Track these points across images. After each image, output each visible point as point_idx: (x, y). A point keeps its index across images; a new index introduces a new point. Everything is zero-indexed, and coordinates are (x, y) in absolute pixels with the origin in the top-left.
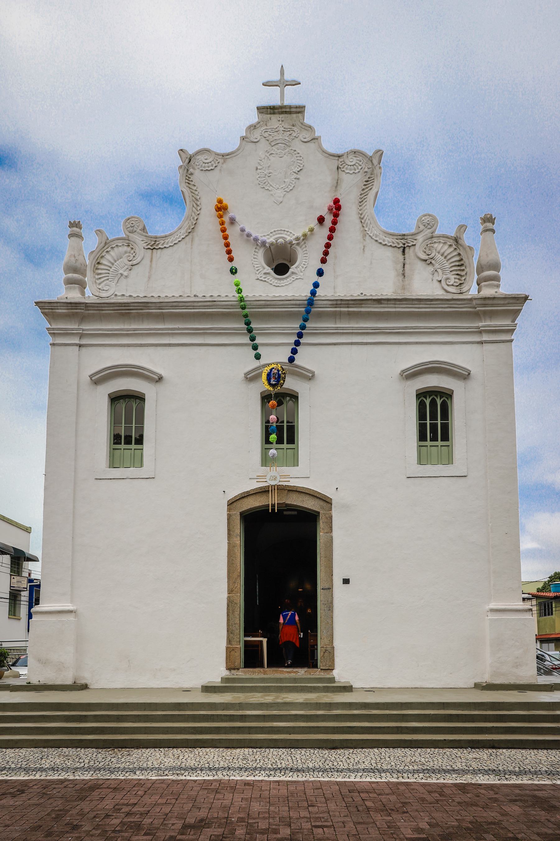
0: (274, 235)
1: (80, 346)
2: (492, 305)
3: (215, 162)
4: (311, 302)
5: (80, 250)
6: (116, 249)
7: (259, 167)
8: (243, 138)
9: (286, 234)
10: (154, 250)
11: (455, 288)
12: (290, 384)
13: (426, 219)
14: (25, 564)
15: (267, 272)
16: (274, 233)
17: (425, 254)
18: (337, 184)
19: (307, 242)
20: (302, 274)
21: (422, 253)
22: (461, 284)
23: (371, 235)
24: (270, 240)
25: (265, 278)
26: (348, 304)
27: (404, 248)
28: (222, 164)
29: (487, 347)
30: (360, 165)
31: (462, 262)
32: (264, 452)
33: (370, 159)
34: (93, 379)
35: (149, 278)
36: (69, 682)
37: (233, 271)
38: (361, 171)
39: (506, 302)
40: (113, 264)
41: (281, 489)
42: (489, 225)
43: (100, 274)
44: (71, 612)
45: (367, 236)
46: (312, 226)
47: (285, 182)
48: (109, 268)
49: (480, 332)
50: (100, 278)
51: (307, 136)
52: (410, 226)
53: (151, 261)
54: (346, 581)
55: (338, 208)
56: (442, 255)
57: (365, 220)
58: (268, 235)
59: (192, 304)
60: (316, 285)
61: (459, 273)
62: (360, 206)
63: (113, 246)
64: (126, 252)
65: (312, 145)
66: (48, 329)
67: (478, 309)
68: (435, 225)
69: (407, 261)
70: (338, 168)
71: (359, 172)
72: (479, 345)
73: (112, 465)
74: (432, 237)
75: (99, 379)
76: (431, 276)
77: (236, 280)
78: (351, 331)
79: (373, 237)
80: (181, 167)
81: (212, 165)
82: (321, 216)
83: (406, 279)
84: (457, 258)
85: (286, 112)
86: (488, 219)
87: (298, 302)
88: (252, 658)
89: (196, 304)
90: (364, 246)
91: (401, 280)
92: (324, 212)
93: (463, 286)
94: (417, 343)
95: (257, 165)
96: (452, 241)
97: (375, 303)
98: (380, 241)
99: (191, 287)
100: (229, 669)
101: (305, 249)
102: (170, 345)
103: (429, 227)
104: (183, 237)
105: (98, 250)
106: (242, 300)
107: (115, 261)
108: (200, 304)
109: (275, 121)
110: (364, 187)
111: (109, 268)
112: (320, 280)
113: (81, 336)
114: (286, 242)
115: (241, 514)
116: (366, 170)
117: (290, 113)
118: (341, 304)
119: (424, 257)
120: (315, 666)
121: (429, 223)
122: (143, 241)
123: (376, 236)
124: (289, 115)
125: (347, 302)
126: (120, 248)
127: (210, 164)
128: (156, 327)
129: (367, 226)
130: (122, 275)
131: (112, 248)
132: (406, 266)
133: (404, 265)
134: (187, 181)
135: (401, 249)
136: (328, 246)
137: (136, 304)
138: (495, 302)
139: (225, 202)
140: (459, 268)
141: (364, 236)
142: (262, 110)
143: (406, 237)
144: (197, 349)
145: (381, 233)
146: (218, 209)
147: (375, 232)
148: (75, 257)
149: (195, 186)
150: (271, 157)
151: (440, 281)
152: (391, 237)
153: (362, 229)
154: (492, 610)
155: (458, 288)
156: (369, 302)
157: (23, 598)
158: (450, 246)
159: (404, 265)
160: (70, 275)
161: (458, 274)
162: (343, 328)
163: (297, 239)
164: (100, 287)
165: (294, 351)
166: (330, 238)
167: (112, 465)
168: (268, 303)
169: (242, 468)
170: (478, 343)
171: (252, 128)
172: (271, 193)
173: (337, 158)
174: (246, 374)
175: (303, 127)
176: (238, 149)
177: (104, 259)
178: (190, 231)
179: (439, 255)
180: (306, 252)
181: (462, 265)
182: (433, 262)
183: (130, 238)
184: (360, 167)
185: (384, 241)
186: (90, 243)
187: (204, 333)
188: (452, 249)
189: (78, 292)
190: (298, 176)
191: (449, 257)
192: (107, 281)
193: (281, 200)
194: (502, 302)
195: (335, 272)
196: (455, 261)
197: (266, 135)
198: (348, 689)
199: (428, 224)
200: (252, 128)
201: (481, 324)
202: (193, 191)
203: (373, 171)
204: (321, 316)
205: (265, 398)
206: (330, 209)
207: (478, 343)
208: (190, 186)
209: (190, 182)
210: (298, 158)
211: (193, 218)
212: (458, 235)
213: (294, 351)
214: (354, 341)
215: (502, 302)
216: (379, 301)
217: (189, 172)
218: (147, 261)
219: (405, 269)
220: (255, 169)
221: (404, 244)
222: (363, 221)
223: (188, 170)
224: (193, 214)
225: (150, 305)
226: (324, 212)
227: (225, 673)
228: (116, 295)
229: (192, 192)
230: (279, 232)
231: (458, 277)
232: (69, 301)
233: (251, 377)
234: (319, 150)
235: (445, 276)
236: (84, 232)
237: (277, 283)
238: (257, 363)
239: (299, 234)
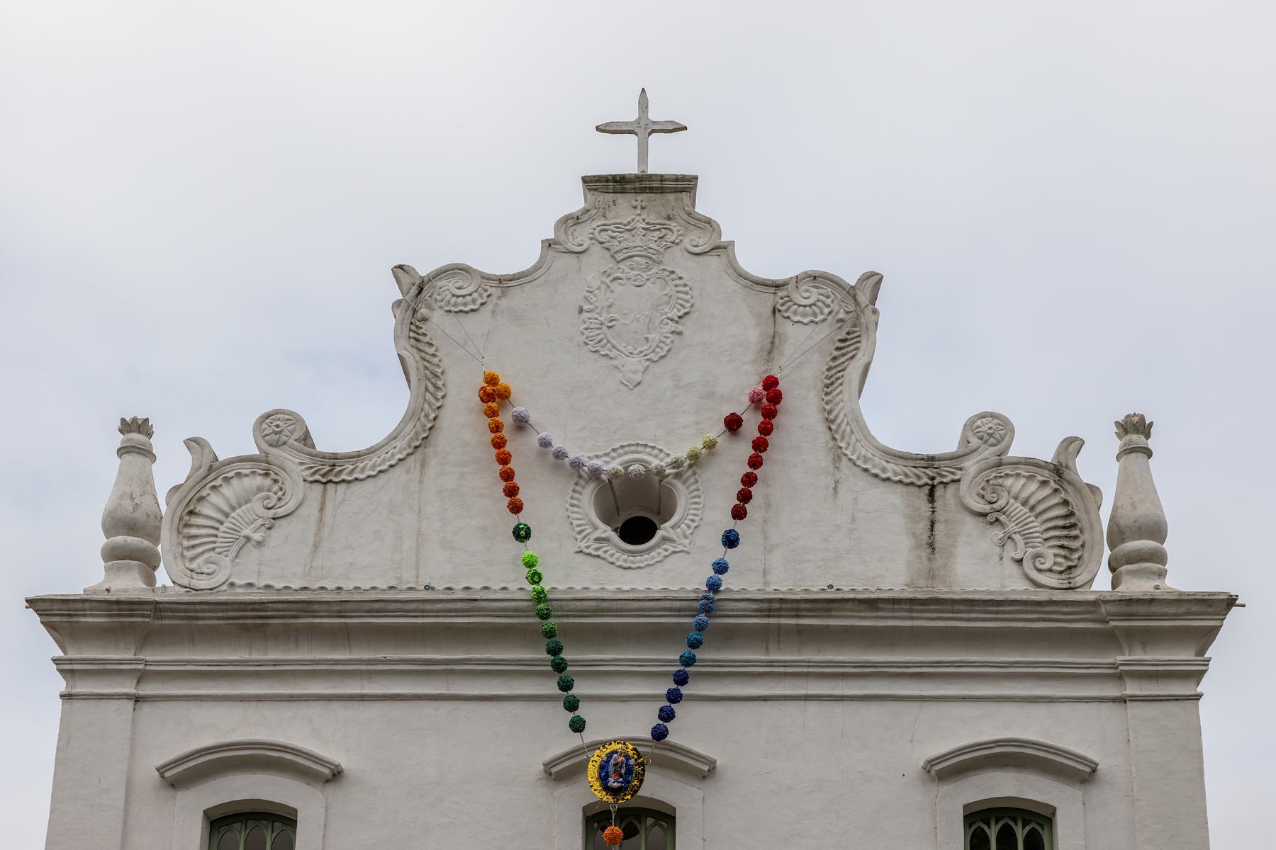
0: (620, 456)
1: (138, 699)
2: (1148, 617)
3: (480, 295)
5: (147, 482)
6: (235, 482)
7: (585, 308)
8: (548, 244)
9: (649, 454)
10: (330, 486)
11: (1057, 576)
12: (656, 787)
15: (604, 535)
16: (621, 451)
17: (982, 501)
18: (772, 346)
19: (699, 471)
20: (687, 542)
21: (976, 498)
22: (1070, 568)
23: (854, 457)
25: (598, 549)
26: (797, 610)
27: (933, 486)
28: (499, 298)
29: (1134, 709)
30: (828, 306)
31: (1073, 520)
33: (851, 292)
34: (167, 775)
35: (316, 546)
37: (522, 534)
38: (830, 318)
39: (1182, 610)
40: (227, 515)
42: (1137, 439)
43: (195, 537)
45: (844, 460)
46: (712, 435)
47: (647, 339)
48: (216, 525)
50: (193, 547)
52: (945, 442)
53: (322, 510)
55: (776, 398)
56: (1024, 503)
57: (839, 425)
58: (606, 455)
59: (420, 606)
60: (721, 568)
61: (1066, 543)
62: (827, 394)
63: (229, 475)
64: (260, 489)
65: (713, 261)
66: (56, 661)
67: (1113, 623)
68: (1007, 438)
69: (940, 516)
70: (774, 312)
71: (825, 320)
72: (1116, 705)
74: (1000, 464)
76: (998, 550)
77: (527, 553)
78: (805, 670)
79: (859, 463)
80: (397, 304)
81: (474, 301)
82: (733, 414)
83: (937, 556)
84: (1061, 511)
85: (652, 190)
87: (677, 604)
89: (428, 606)
90: (837, 482)
91: (925, 558)
92: (740, 406)
93: (1075, 573)
94: (964, 699)
95: (582, 303)
96: (1047, 473)
97: (862, 607)
98: (874, 471)
99: (417, 569)
101: (694, 487)
102: (362, 698)
103: (992, 441)
104: (401, 456)
105: (191, 483)
106: (540, 597)
107: (233, 509)
108: (439, 606)
109: (625, 209)
110: (836, 353)
111: (216, 525)
112: (731, 556)
114: (648, 471)
116: (842, 315)
117: (662, 191)
118: (780, 610)
119: (980, 506)
121: (990, 431)
122: (301, 464)
123: (866, 460)
124: (658, 196)
125: (795, 606)
126: (246, 480)
127: (468, 298)
128: (329, 657)
129: (843, 439)
130: (248, 539)
131: (227, 479)
132: (937, 526)
133: (933, 524)
134: (412, 334)
135: (926, 490)
136: (749, 480)
137: (281, 606)
138: (1155, 609)
139: (503, 381)
140: (1065, 533)
141: (837, 459)
142: (593, 184)
143: (936, 464)
144: (428, 708)
145: (877, 453)
146: (487, 397)
147: (864, 452)
148: (132, 498)
149: (431, 345)
150: (615, 286)
151: (1020, 561)
152: (901, 462)
153: (831, 444)
155: (1063, 576)
156: (849, 605)
158: (1044, 483)
159: (933, 524)
160: (119, 539)
161: (1062, 547)
162: (785, 664)
163: (677, 464)
164: (194, 566)
165: (667, 715)
166: (755, 462)
168: (605, 604)
170: (1114, 700)
171: (571, 222)
172: (614, 362)
173: (772, 290)
174: (548, 765)
175: (693, 221)
176: (536, 268)
177: (205, 503)
178: (417, 443)
179: (1017, 504)
180: (696, 493)
181: (1073, 526)
182: (1003, 518)
183: (271, 458)
184: (826, 310)
185: (884, 470)
186: (171, 469)
187: (448, 671)
189: (137, 576)
190: (680, 328)
191: (1040, 508)
192: (212, 554)
193: (638, 378)
194: (1172, 610)
195: (765, 538)
196: (1057, 517)
197: (604, 237)
199: (991, 435)
200: (570, 222)
201: (1120, 658)
202: (428, 357)
203: (858, 317)
204: (732, 636)
206: (755, 400)
207: (1114, 700)
208: (419, 345)
209: (420, 337)
210: (680, 289)
211: (426, 416)
212: (1063, 460)
213: (667, 715)
214: (811, 692)
215: (1172, 610)
216: (872, 604)
217: (418, 315)
218: (311, 510)
219: (936, 532)
220: (577, 310)
221: (933, 479)
222: (833, 427)
223: (415, 311)
224: (426, 407)
225: (315, 607)
226: (740, 406)
228: (232, 585)
229: (424, 359)
230: (634, 448)
231: (1062, 552)
232: (114, 598)
233: (561, 772)
234: (730, 271)
235: (1030, 550)
236: (156, 443)
237: (625, 561)
238: (575, 741)
239: (681, 452)
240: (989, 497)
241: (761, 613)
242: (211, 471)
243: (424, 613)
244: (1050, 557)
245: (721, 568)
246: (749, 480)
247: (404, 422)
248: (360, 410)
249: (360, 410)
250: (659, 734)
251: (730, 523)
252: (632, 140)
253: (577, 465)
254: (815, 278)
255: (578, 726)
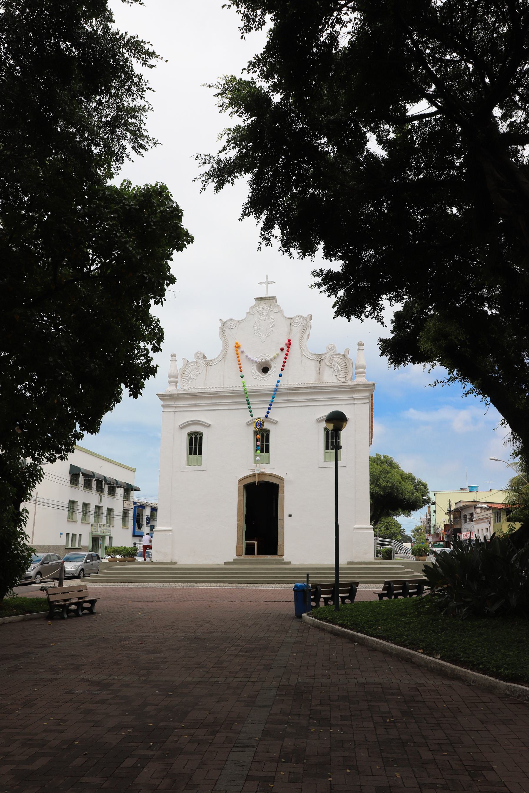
4: (276, 390)
8: (248, 313)
12: (266, 426)
13: (330, 347)
14: (132, 492)
18: (290, 332)
24: (259, 360)
32: (256, 456)
33: (305, 319)
36: (169, 561)
41: (261, 474)
42: (361, 347)
44: (170, 530)
46: (278, 352)
49: (354, 399)
51: (276, 310)
54: (290, 516)
55: (290, 344)
60: (278, 382)
65: (279, 314)
69: (321, 367)
73: (188, 465)
75: (182, 427)
84: (344, 364)
86: (361, 344)
88: (249, 551)
100: (237, 555)
106: (245, 390)
113: (176, 407)
115: (244, 486)
119: (329, 364)
120: (277, 555)
136: (284, 362)
139: (239, 344)
142: (256, 299)
146: (236, 347)
154: (355, 528)
157: (130, 515)
160: (171, 379)
165: (268, 413)
166: (286, 358)
167: (188, 465)
169: (245, 464)
171: (252, 307)
174: (247, 423)
186: (180, 364)
188: (342, 360)
198: (289, 563)
201: (354, 396)
204: (281, 395)
205: (256, 433)
206: (286, 344)
213: (268, 413)
227: (235, 557)
233: (249, 424)
239: (272, 357)
240: (331, 362)
241: (286, 390)
242: (187, 363)
243: (225, 393)
244: (342, 374)
245: (278, 382)
246: (284, 362)
247: (221, 352)
248: (213, 349)
249: (213, 352)
250: (267, 417)
251: (280, 372)
252: (269, 281)
253: (253, 361)
254: (298, 316)
255: (252, 416)
